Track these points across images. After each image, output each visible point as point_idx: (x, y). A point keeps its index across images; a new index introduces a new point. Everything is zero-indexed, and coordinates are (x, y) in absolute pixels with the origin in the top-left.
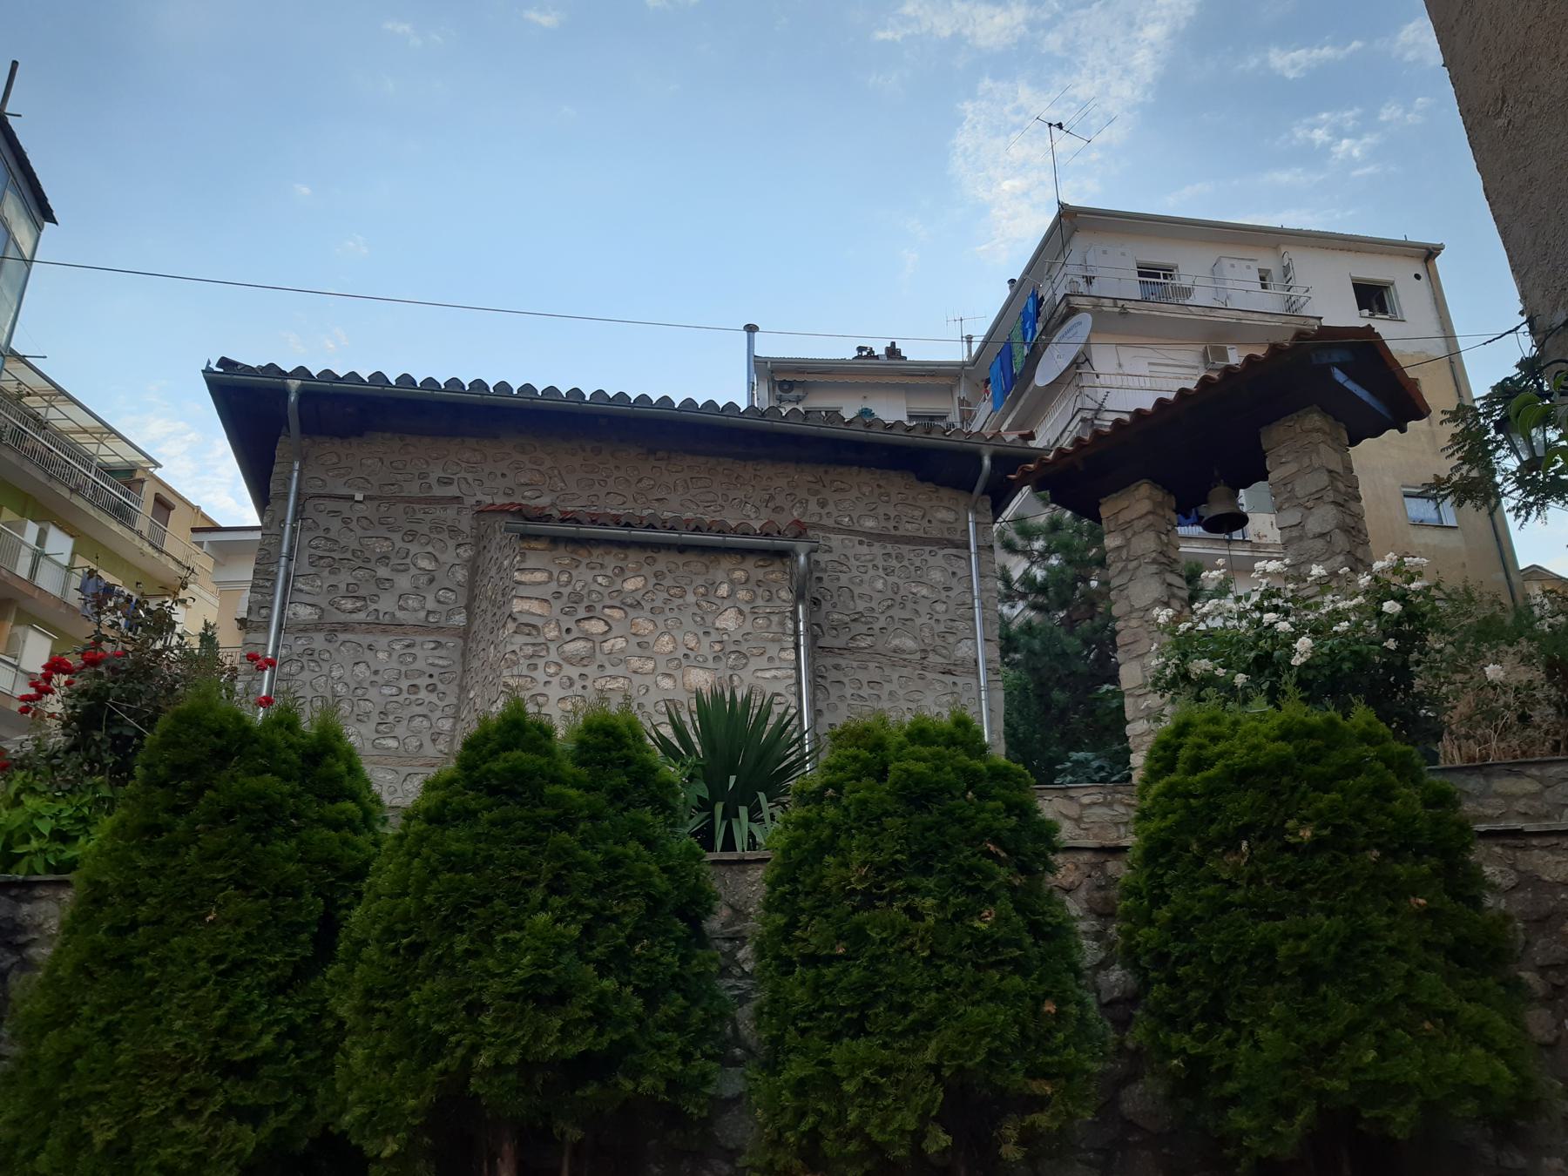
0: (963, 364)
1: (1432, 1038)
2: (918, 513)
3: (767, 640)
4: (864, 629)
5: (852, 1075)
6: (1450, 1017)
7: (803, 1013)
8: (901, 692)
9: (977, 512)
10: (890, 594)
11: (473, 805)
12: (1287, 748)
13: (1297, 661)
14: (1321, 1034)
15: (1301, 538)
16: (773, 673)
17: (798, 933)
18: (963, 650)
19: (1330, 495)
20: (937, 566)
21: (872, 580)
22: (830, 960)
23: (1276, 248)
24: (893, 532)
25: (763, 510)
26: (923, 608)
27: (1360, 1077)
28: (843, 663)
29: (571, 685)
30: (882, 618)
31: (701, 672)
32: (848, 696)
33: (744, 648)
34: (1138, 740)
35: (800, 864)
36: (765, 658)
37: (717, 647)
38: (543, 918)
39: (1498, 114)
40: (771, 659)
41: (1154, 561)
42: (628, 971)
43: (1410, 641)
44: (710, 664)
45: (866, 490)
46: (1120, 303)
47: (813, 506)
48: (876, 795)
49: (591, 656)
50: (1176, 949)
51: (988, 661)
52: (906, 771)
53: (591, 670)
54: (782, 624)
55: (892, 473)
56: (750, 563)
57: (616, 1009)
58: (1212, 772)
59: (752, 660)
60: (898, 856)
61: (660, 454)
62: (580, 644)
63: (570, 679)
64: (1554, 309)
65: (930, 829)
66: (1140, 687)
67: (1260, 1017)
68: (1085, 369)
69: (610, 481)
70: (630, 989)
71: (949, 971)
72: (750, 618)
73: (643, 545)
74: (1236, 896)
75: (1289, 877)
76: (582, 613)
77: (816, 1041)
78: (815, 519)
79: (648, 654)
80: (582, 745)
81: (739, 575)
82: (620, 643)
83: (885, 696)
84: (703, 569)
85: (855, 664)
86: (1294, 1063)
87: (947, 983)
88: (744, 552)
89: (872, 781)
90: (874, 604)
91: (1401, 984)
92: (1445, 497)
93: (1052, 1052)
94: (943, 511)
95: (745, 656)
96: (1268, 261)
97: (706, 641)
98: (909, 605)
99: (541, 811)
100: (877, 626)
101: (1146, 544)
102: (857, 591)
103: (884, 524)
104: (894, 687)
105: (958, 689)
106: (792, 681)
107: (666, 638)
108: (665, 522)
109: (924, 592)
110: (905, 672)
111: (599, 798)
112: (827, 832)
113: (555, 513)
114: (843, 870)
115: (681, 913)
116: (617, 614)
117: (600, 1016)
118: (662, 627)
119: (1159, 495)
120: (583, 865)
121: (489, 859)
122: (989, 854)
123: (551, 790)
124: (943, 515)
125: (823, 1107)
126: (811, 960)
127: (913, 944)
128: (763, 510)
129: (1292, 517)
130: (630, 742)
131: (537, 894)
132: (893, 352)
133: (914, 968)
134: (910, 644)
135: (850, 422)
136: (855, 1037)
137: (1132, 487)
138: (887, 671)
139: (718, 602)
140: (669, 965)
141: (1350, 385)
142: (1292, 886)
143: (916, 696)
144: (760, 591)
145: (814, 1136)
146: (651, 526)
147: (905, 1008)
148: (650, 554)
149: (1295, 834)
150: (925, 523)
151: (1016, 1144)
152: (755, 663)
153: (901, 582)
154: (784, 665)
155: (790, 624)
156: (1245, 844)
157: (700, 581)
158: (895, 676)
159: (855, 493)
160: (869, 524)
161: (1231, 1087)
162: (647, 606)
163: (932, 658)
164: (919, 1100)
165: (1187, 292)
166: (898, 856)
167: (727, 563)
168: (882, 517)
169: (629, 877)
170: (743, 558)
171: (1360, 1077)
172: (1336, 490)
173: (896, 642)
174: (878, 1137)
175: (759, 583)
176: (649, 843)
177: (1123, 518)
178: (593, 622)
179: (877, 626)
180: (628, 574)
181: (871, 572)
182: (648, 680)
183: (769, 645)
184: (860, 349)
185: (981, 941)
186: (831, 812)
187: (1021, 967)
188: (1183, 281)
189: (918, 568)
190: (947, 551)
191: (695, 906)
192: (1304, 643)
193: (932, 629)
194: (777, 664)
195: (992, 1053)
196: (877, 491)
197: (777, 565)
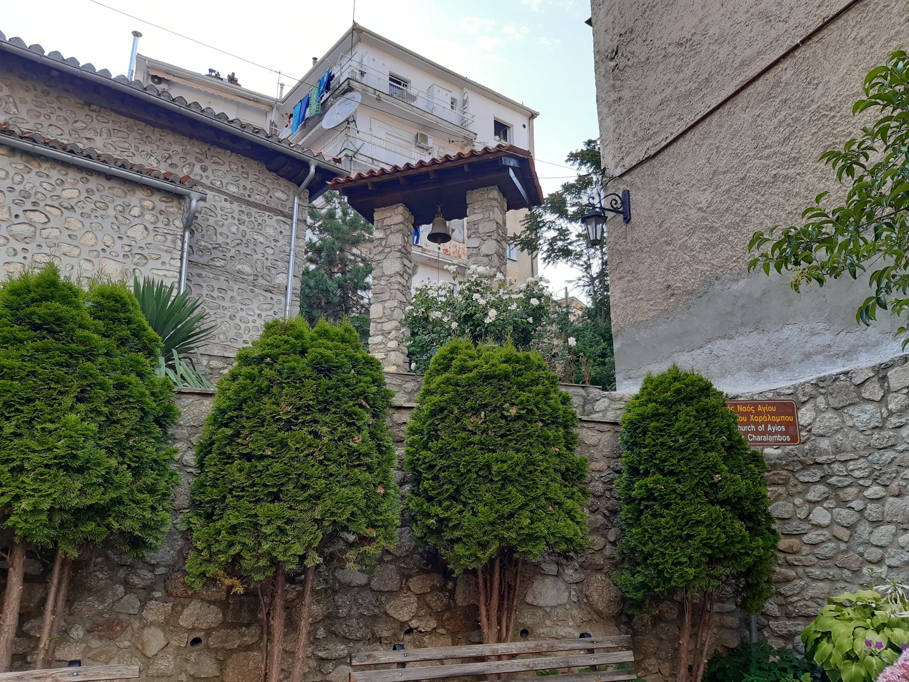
0: (276, 101)
1: (552, 515)
2: (264, 190)
3: (162, 250)
4: (220, 255)
5: (269, 523)
6: (560, 504)
7: (238, 487)
8: (238, 298)
9: (300, 198)
10: (240, 236)
11: (20, 335)
12: (509, 368)
13: (487, 321)
14: (507, 509)
15: (477, 255)
16: (164, 272)
17: (239, 440)
18: (280, 279)
19: (495, 236)
20: (272, 224)
21: (231, 224)
22: (261, 458)
23: (462, 88)
24: (247, 198)
25: (162, 163)
26: (260, 249)
27: (522, 532)
28: (204, 273)
29: (15, 255)
30: (233, 251)
31: (113, 263)
32: (204, 295)
33: (145, 252)
34: (374, 347)
35: (245, 401)
36: (160, 261)
37: (127, 249)
38: (73, 417)
39: (612, 59)
40: (163, 263)
41: (399, 251)
42: (123, 455)
43: (537, 320)
44: (120, 258)
45: (234, 167)
46: (378, 93)
47: (197, 169)
48: (301, 365)
49: (33, 237)
50: (440, 463)
51: (294, 289)
52: (320, 354)
53: (32, 247)
54: (174, 242)
55: (252, 161)
56: (156, 198)
57: (116, 478)
58: (470, 375)
59: (150, 261)
60: (311, 402)
61: (93, 107)
62: (25, 228)
63: (14, 250)
64: (616, 167)
65: (330, 388)
66: (381, 318)
67: (478, 500)
68: (352, 125)
69: (53, 117)
70: (125, 466)
71: (333, 468)
72: (152, 234)
73: (80, 168)
74: (476, 438)
75: (503, 431)
76: (28, 206)
77: (244, 503)
78: (198, 178)
79: (75, 243)
80: (98, 305)
81: (148, 204)
82: (56, 232)
83: (227, 299)
84: (123, 195)
85: (211, 276)
86: (492, 524)
87: (331, 475)
88: (154, 189)
89: (298, 357)
90: (229, 241)
91: (544, 488)
92: (516, 245)
93: (381, 514)
94: (280, 193)
95: (146, 258)
96: (456, 94)
97: (119, 243)
98: (251, 246)
99: (73, 346)
100: (229, 255)
101: (396, 240)
102: (219, 231)
103: (242, 191)
104: (234, 294)
105: (273, 302)
106: (177, 280)
107: (90, 235)
108: (99, 156)
109: (261, 239)
110: (242, 286)
111: (112, 343)
112: (266, 383)
113: (16, 130)
114: (274, 407)
115: (157, 421)
116: (55, 212)
117: (107, 481)
118: (87, 227)
119: (407, 214)
120: (103, 386)
121: (33, 373)
122: (361, 406)
123: (79, 332)
124: (279, 194)
125: (247, 541)
126: (249, 457)
127: (314, 452)
128: (162, 163)
129: (474, 242)
130: (131, 308)
131: (68, 401)
132: (232, 79)
133: (313, 466)
134: (248, 269)
135: (232, 121)
136: (272, 502)
137: (394, 206)
138: (231, 284)
139: (131, 218)
140: (151, 453)
141: (515, 180)
142: (502, 436)
143: (247, 302)
144: (161, 218)
145: (238, 557)
146: (89, 157)
147: (304, 487)
148: (84, 175)
149: (508, 411)
150: (268, 197)
151: (355, 562)
152: (152, 264)
153: (248, 231)
154: (172, 268)
155: (179, 243)
156: (483, 413)
157: (119, 201)
158: (236, 288)
159: (226, 167)
160: (233, 189)
161: (457, 534)
162: (79, 211)
163: (260, 280)
164: (306, 538)
165: (414, 98)
166: (311, 402)
167: (140, 194)
168: (241, 187)
169: (130, 396)
170: (152, 193)
171: (522, 532)
172: (498, 234)
173: (239, 267)
174: (281, 558)
175: (161, 212)
176: (140, 375)
177: (386, 222)
178: (36, 213)
179: (229, 255)
180: (66, 186)
181: (230, 220)
182: (74, 261)
183: (163, 254)
184: (211, 71)
185: (352, 452)
186: (267, 372)
187: (370, 469)
188: (412, 91)
189: (259, 224)
190: (279, 218)
191: (165, 418)
192: (493, 313)
193: (263, 263)
194: (167, 267)
195: (353, 514)
196: (240, 170)
197: (175, 203)
